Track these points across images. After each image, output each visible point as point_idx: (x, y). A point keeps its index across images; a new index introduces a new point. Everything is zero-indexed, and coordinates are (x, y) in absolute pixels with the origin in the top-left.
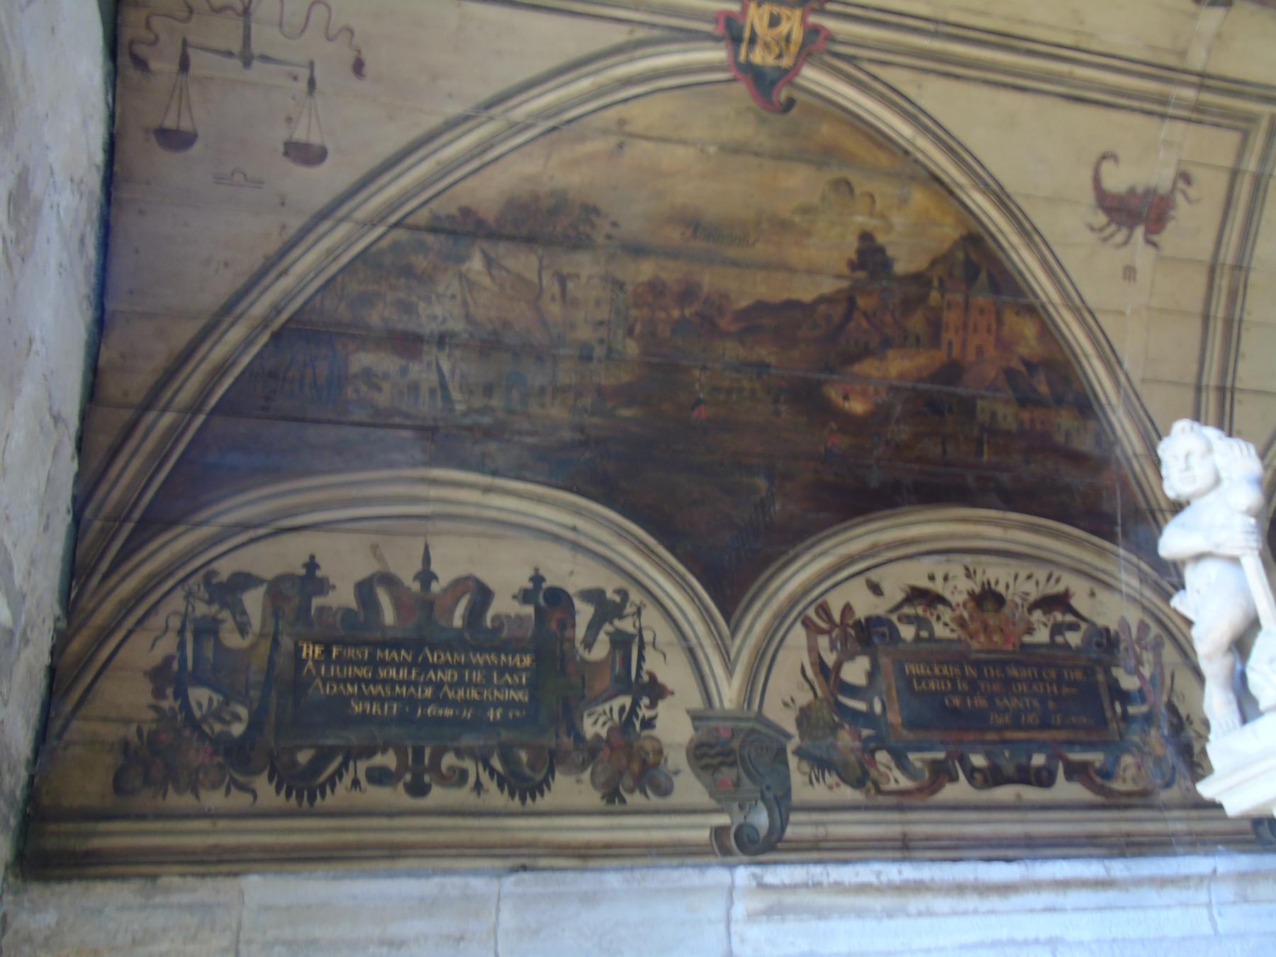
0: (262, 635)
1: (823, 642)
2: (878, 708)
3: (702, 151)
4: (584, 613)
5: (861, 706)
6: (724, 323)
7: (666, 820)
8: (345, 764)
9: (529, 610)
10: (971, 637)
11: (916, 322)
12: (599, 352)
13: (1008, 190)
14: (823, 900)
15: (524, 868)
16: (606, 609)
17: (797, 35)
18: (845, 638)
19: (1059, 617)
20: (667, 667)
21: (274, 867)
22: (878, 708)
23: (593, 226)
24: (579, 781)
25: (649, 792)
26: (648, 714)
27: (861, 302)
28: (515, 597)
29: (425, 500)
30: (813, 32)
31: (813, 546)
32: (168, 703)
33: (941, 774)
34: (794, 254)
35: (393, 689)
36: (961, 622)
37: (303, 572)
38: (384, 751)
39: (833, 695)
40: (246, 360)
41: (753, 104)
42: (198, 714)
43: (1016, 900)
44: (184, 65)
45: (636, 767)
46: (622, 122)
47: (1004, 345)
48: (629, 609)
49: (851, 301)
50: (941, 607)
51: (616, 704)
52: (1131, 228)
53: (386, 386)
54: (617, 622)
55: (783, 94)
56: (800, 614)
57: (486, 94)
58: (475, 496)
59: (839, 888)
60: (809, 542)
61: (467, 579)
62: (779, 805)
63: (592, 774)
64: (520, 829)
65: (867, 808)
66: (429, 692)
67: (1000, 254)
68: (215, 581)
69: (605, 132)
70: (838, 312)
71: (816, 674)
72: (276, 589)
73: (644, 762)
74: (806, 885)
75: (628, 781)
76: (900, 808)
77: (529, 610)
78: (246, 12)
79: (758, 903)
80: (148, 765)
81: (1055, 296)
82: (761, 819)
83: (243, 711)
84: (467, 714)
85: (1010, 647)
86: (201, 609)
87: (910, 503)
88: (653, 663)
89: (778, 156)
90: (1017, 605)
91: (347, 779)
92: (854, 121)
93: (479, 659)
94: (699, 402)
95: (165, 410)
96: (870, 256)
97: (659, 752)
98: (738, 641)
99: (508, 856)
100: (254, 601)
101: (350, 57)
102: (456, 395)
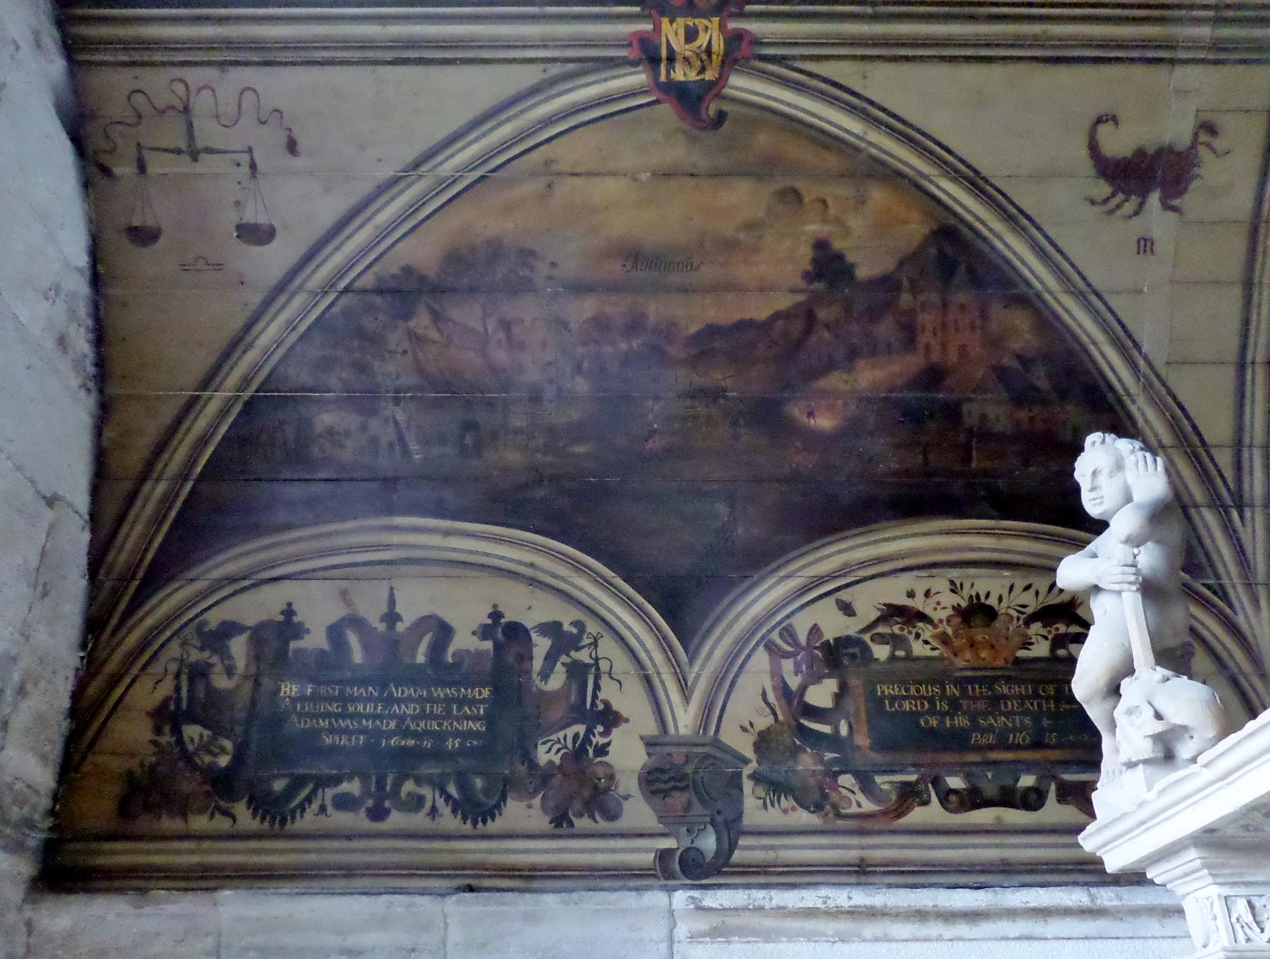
0: (246, 677)
1: (787, 665)
2: (844, 731)
3: (635, 179)
4: (541, 645)
5: (826, 729)
6: (676, 351)
7: (612, 843)
8: (314, 791)
9: (488, 645)
10: (955, 655)
11: (885, 329)
12: (549, 392)
13: (984, 172)
14: (769, 923)
15: (471, 889)
16: (563, 641)
17: (718, 46)
18: (812, 660)
19: (1062, 628)
20: (624, 696)
21: (244, 883)
22: (844, 731)
23: (532, 269)
24: (530, 807)
25: (598, 817)
26: (602, 741)
27: (823, 314)
28: (474, 633)
29: (389, 547)
30: (735, 40)
31: (779, 568)
32: (167, 739)
33: (909, 796)
34: (744, 273)
35: (360, 723)
36: (945, 640)
37: (281, 618)
38: (350, 778)
39: (796, 720)
40: (223, 429)
41: (685, 126)
42: (190, 748)
43: (986, 928)
44: (142, 168)
45: (587, 793)
46: (548, 163)
47: (995, 343)
48: (586, 641)
49: (810, 318)
50: (920, 625)
51: (570, 732)
52: (1144, 195)
53: (349, 443)
54: (573, 653)
55: (713, 108)
56: (763, 638)
57: (411, 155)
58: (436, 540)
59: (781, 911)
60: (774, 565)
61: (428, 618)
62: (728, 829)
63: (543, 798)
64: (467, 851)
65: (823, 832)
66: (393, 725)
67: (980, 244)
68: (206, 629)
69: (533, 175)
70: (797, 327)
71: (778, 699)
72: (258, 635)
73: (596, 787)
74: (746, 909)
75: (578, 805)
76: (862, 833)
77: (488, 645)
78: (186, 110)
79: (703, 924)
80: (146, 795)
81: (1051, 282)
82: (709, 843)
83: (228, 745)
84: (428, 744)
85: (1000, 663)
86: (195, 656)
87: (888, 519)
88: (608, 691)
89: (714, 175)
90: (1011, 618)
91: (315, 806)
92: (792, 124)
93: (440, 693)
94: (653, 433)
95: (158, 480)
96: (828, 266)
97: (611, 777)
98: (696, 668)
99: (457, 876)
100: (239, 647)
101: (282, 138)
102: (414, 446)
